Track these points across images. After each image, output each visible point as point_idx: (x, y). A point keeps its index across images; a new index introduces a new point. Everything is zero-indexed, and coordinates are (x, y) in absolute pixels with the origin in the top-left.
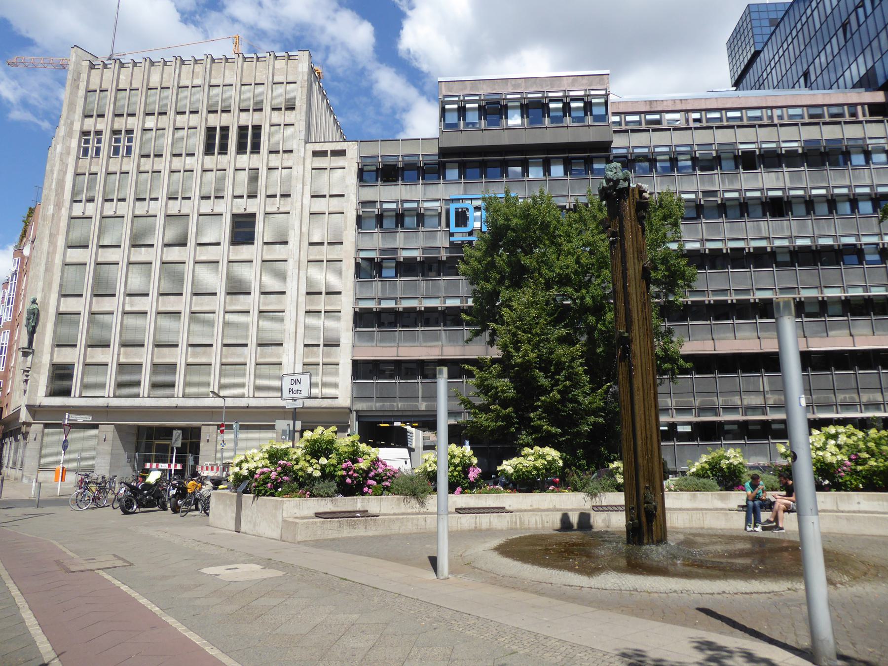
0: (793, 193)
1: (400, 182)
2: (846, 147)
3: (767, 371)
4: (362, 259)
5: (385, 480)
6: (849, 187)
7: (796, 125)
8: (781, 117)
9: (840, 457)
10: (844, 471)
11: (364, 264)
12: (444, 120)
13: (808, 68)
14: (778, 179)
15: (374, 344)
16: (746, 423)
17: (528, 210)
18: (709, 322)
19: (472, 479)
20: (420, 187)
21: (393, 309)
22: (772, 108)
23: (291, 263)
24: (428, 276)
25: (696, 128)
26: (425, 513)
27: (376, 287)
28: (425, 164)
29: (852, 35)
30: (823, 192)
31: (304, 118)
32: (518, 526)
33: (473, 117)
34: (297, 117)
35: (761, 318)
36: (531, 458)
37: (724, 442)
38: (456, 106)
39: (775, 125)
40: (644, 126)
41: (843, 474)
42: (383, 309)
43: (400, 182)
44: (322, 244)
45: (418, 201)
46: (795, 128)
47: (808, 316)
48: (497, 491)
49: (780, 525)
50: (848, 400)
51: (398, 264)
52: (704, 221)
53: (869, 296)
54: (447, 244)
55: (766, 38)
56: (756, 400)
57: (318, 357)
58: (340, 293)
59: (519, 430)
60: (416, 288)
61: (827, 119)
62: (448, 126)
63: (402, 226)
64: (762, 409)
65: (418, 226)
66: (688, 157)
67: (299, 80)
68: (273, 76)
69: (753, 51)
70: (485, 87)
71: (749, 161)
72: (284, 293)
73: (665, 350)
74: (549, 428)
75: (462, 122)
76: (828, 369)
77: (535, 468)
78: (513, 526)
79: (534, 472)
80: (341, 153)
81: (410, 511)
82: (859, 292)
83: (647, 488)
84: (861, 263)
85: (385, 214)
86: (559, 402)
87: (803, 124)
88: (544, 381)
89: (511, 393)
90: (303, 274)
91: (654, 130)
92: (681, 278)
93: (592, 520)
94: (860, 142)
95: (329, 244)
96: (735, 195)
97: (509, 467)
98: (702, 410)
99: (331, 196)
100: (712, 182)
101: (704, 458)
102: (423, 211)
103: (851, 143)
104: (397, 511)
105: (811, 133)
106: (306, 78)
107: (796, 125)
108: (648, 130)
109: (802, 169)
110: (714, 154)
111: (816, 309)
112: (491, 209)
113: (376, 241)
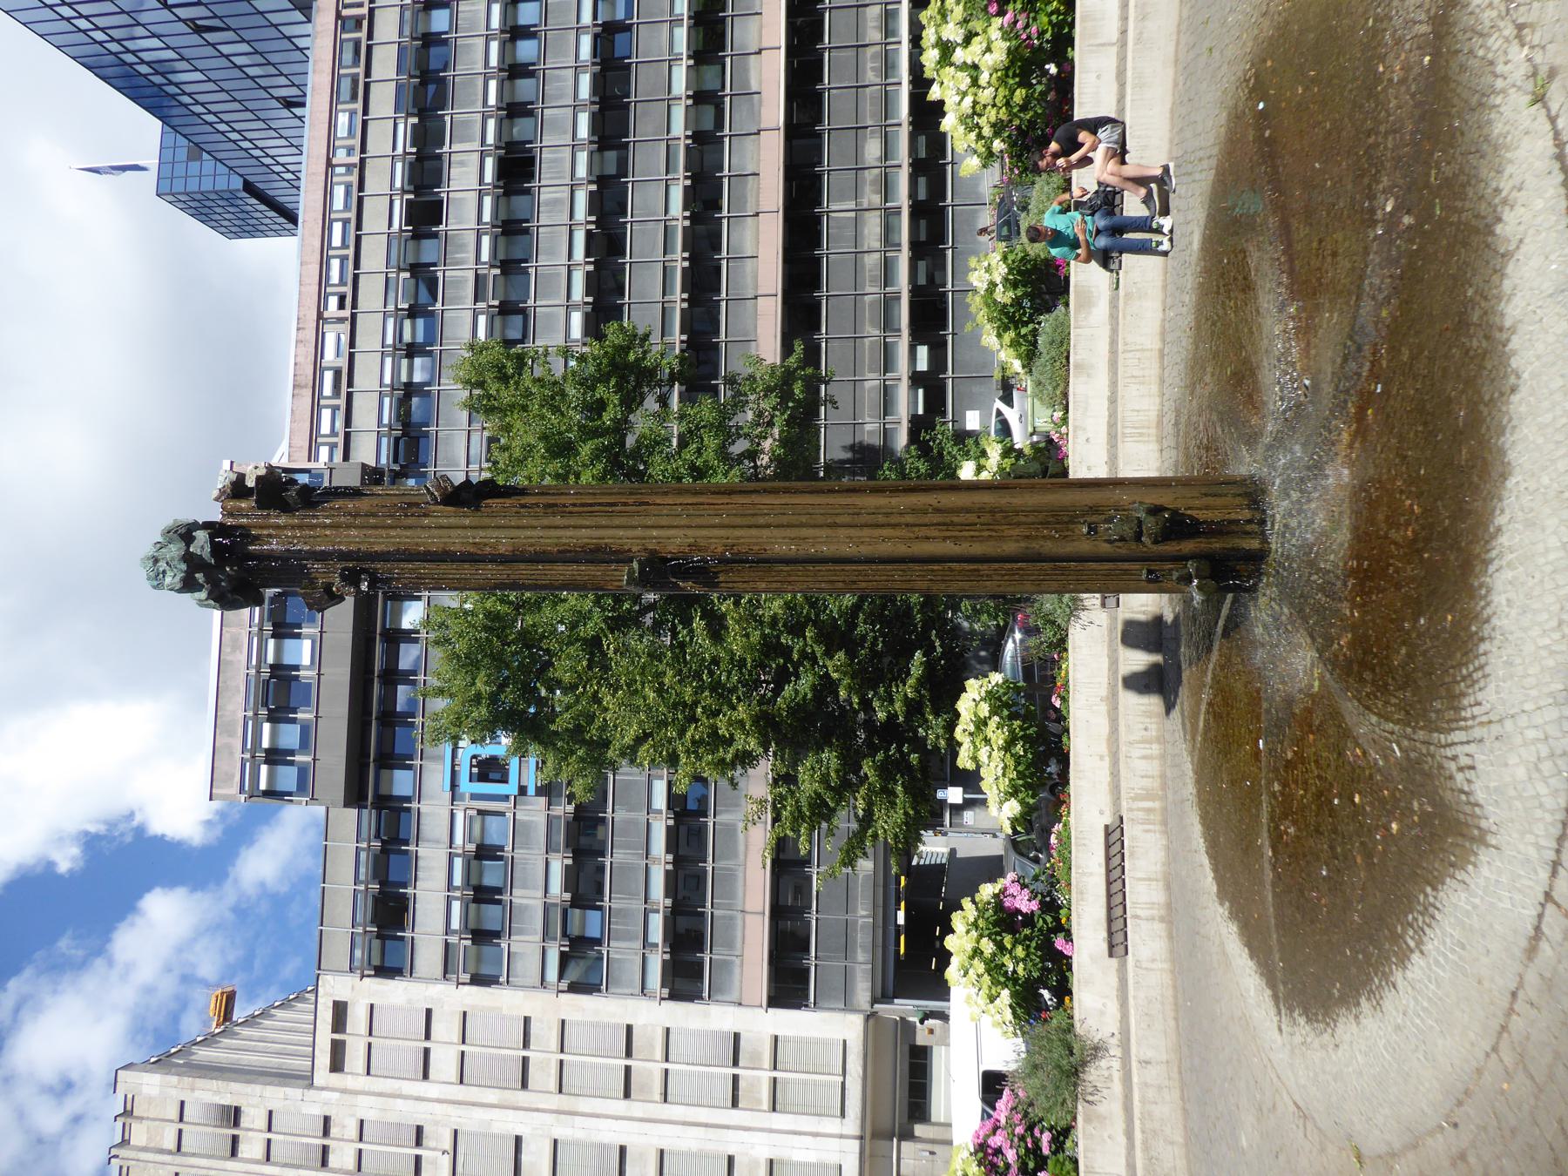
0: (490, 139)
1: (410, 891)
2: (413, 39)
3: (820, 204)
4: (561, 977)
5: (1036, 1142)
6: (488, 39)
7: (365, 123)
8: (350, 151)
9: (994, 33)
10: (1027, 26)
11: (574, 973)
12: (290, 794)
13: (277, 99)
14: (462, 164)
15: (737, 961)
16: (914, 245)
17: (458, 657)
18: (723, 304)
19: (1034, 906)
20: (422, 851)
21: (665, 918)
22: (329, 164)
23: (558, 1133)
24: (604, 842)
25: (354, 306)
26: (1125, 1044)
27: (621, 952)
28: (377, 836)
29: (215, 16)
30: (493, 85)
31: (257, 1089)
32: (1156, 805)
33: (290, 736)
34: (255, 1100)
35: (720, 209)
36: (983, 754)
37: (949, 286)
38: (264, 769)
39: (362, 161)
40: (342, 402)
41: (1034, 28)
42: (665, 940)
43: (410, 891)
44: (525, 1060)
45: (451, 857)
46: (371, 126)
47: (719, 124)
48: (1065, 841)
49: (1158, 172)
50: (877, 65)
51: (577, 902)
52: (531, 302)
53: (690, 18)
54: (543, 800)
55: (221, 168)
56: (872, 227)
57: (759, 1079)
58: (629, 1028)
59: (919, 744)
60: (627, 869)
61: (361, 70)
62: (302, 787)
63: (499, 891)
64: (890, 215)
65: (501, 858)
66: (407, 323)
67: (177, 1095)
68: (162, 1151)
69: (245, 195)
70: (230, 707)
71: (425, 214)
72: (623, 1150)
73: (768, 390)
74: (911, 681)
75: (298, 758)
76: (820, 95)
77: (1008, 747)
78: (1158, 818)
79: (1019, 749)
80: (340, 1011)
81: (1117, 1087)
82: (682, 34)
83: (1093, 529)
84: (629, 28)
85: (472, 925)
86: (852, 654)
87: (365, 112)
88: (805, 684)
89: (830, 758)
90: (585, 1105)
91: (350, 384)
92: (627, 354)
93: (1142, 617)
94: (408, 14)
95: (526, 1045)
96: (486, 241)
97: (1007, 805)
98: (888, 324)
99: (428, 1037)
100: (460, 282)
101: (990, 339)
102: (472, 847)
103: (407, 32)
104: (1119, 1126)
105: (383, 99)
106: (174, 1079)
107: (365, 123)
108: (350, 396)
109: (448, 118)
110: (407, 275)
111: (709, 111)
112: (454, 730)
113: (528, 946)
